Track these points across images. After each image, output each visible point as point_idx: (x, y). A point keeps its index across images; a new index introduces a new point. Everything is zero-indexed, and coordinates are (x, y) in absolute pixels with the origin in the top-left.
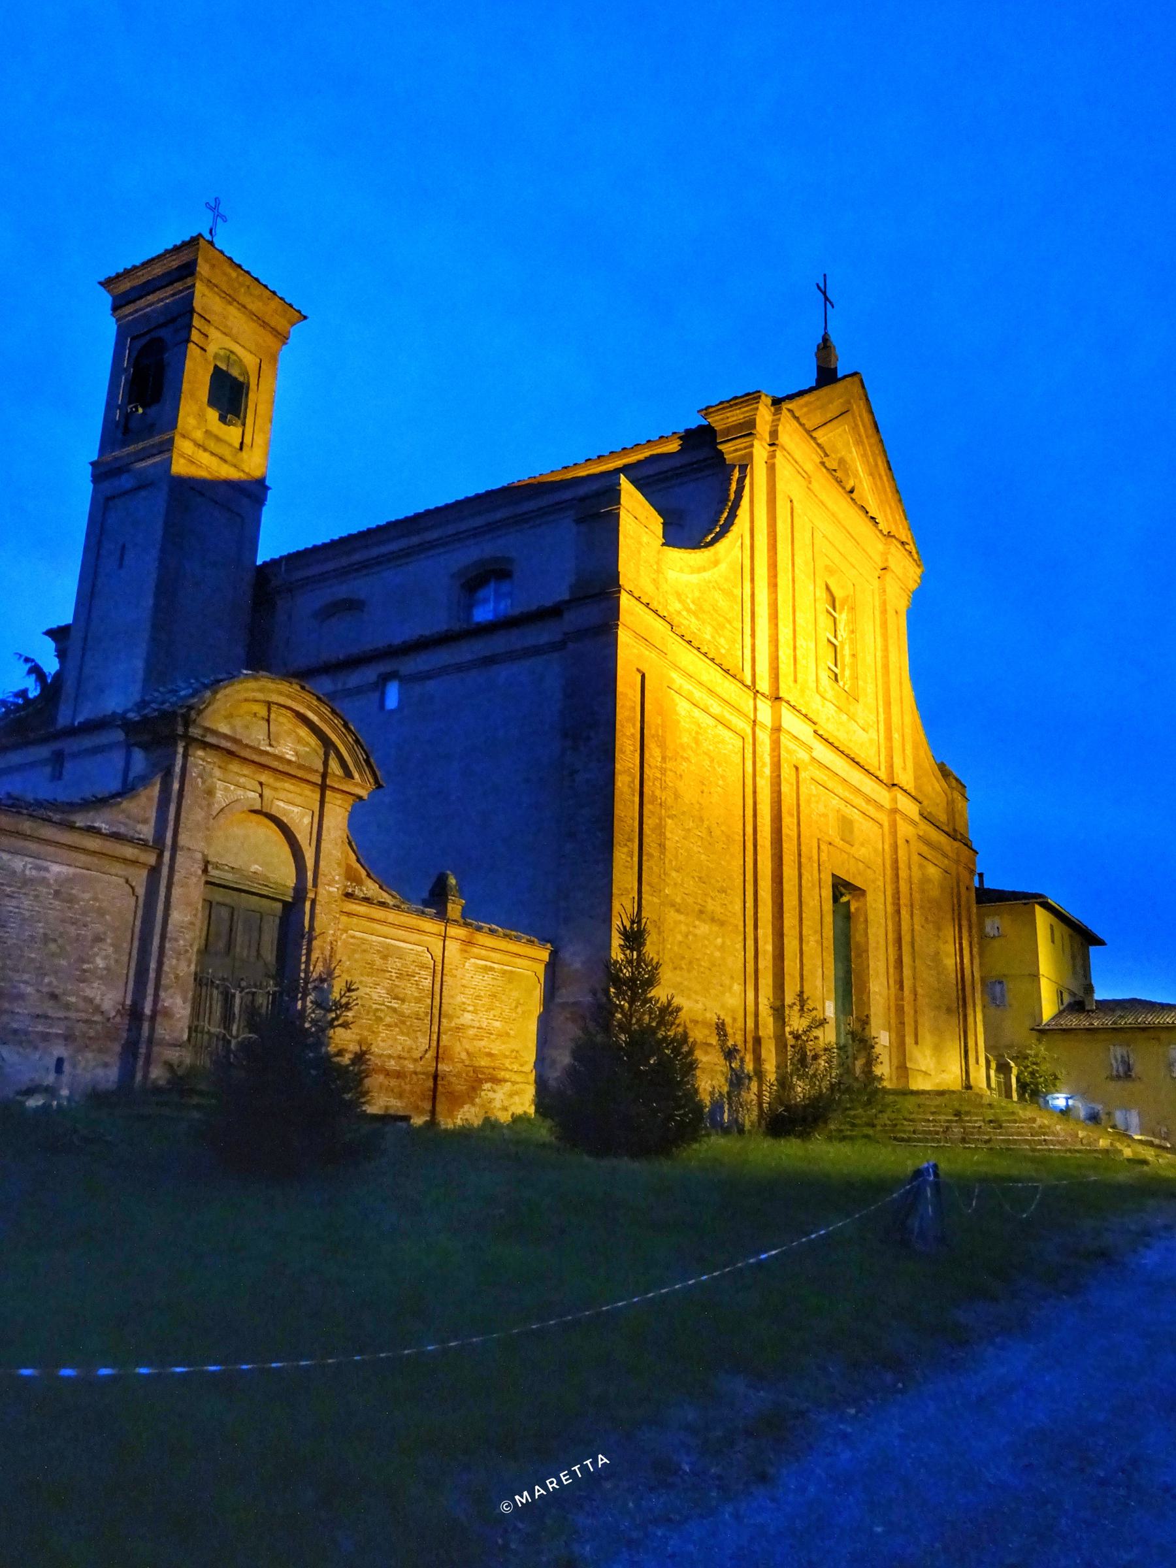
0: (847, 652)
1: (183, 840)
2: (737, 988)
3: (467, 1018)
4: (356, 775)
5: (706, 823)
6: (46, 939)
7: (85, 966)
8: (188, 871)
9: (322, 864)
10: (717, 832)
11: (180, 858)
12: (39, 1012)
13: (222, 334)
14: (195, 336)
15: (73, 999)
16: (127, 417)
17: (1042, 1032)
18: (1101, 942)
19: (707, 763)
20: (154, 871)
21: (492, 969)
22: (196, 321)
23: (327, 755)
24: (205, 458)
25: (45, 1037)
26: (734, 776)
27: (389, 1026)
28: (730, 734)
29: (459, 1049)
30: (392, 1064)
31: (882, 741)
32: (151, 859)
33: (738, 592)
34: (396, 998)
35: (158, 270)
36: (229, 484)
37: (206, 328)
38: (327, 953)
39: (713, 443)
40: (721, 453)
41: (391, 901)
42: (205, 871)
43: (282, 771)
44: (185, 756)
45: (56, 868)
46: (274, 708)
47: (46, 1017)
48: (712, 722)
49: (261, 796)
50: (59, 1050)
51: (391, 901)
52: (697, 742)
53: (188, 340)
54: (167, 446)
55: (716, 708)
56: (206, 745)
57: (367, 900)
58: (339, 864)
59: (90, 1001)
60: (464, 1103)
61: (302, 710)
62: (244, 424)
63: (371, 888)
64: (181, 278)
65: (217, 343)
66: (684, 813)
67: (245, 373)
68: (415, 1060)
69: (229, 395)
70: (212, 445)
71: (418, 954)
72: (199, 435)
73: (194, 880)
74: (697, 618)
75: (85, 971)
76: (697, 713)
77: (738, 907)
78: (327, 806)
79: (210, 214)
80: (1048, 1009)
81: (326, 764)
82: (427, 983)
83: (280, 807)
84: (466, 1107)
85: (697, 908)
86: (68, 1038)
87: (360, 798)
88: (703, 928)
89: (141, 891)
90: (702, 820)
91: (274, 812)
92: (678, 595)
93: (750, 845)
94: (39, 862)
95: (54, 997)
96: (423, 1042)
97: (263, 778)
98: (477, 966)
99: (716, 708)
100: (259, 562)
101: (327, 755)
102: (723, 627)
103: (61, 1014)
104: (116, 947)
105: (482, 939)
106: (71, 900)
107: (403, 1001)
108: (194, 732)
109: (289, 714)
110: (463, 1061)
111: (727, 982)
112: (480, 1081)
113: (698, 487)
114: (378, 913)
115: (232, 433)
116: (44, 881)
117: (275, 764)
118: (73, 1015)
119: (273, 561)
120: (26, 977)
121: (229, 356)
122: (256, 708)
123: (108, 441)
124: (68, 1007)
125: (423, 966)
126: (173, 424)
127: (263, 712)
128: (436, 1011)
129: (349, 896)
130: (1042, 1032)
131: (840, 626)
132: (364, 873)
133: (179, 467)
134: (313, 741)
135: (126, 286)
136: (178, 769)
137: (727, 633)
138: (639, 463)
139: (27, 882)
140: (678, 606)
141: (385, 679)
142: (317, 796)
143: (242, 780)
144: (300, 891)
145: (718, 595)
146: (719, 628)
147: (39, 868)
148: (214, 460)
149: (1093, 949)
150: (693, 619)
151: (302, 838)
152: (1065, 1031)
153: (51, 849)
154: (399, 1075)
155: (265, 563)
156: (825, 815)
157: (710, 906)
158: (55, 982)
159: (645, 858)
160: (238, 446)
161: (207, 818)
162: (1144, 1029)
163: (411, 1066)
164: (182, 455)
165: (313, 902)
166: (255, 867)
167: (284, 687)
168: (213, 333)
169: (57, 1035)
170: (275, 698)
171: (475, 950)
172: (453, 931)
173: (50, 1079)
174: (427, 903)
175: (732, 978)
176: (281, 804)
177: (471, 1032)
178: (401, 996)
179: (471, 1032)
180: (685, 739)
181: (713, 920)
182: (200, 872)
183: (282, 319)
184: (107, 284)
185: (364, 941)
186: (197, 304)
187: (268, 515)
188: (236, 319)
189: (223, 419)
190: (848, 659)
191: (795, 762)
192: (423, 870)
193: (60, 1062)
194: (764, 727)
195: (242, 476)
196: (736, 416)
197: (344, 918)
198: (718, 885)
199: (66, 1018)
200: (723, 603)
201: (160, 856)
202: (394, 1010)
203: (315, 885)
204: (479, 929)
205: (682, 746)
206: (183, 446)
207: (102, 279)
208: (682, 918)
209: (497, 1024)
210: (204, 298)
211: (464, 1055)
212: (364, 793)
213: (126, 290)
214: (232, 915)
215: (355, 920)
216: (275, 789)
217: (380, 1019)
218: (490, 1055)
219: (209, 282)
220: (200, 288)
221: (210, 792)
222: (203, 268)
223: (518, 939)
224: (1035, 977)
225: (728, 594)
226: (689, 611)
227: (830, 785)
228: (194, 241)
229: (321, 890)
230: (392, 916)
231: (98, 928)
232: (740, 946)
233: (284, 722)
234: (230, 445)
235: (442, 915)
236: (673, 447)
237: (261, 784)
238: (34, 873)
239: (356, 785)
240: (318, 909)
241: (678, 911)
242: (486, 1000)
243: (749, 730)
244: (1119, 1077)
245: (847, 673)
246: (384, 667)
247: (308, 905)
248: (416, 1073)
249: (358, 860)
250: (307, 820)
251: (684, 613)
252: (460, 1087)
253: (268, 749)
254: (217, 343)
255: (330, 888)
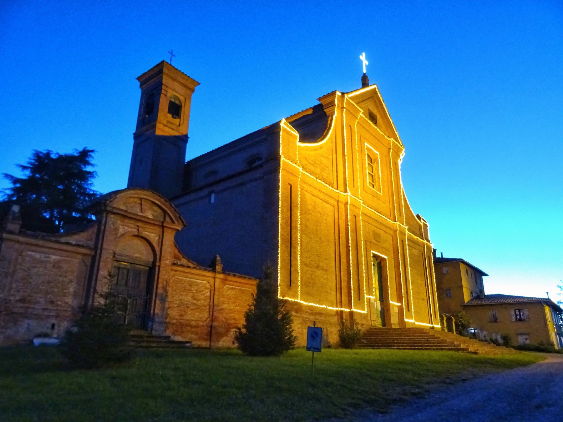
0: (377, 177)
1: (105, 246)
2: (334, 293)
3: (225, 306)
4: (176, 222)
5: (319, 236)
6: (49, 282)
7: (65, 291)
8: (106, 256)
9: (163, 253)
10: (323, 239)
11: (103, 252)
12: (46, 307)
13: (171, 90)
14: (163, 91)
15: (59, 303)
16: (144, 119)
17: (465, 306)
18: (486, 275)
19: (319, 215)
20: (94, 257)
21: (235, 289)
22: (163, 87)
23: (165, 216)
24: (167, 129)
25: (48, 317)
26: (330, 220)
27: (192, 310)
28: (329, 205)
29: (221, 317)
30: (193, 323)
31: (391, 206)
32: (93, 253)
33: (331, 157)
34: (195, 299)
35: (152, 73)
36: (175, 137)
37: (167, 89)
38: (165, 284)
39: (323, 109)
40: (325, 112)
41: (192, 266)
42: (114, 256)
43: (146, 222)
44: (106, 217)
45: (54, 257)
46: (143, 200)
47: (48, 309)
48: (321, 201)
49: (138, 230)
50: (54, 321)
51: (192, 266)
52: (314, 208)
53: (161, 93)
54: (154, 127)
55: (322, 196)
56: (114, 213)
57: (182, 266)
58: (170, 253)
59: (67, 303)
60: (224, 336)
61: (154, 200)
62: (180, 118)
63: (184, 261)
64: (159, 74)
65: (170, 93)
66: (309, 233)
67: (180, 101)
68: (203, 322)
69: (176, 110)
70: (169, 125)
71: (204, 284)
72: (165, 122)
73: (109, 260)
74: (314, 166)
75: (65, 293)
76: (314, 198)
77: (333, 264)
78: (165, 234)
79: (170, 55)
80: (467, 298)
81: (165, 219)
82: (208, 294)
83: (146, 234)
84: (224, 338)
85: (316, 265)
86: (57, 317)
87: (178, 230)
88: (319, 272)
89: (89, 264)
90: (317, 235)
91: (143, 235)
92: (306, 159)
93: (337, 243)
94: (47, 255)
95: (52, 302)
96: (206, 315)
97: (139, 224)
98: (228, 287)
99: (322, 196)
100: (186, 161)
101: (165, 216)
102: (325, 169)
103: (55, 308)
104: (78, 284)
105: (230, 278)
106: (60, 267)
107: (198, 300)
108: (108, 208)
109: (149, 202)
110: (223, 321)
111: (329, 291)
112: (230, 328)
113: (313, 124)
114: (188, 270)
115: (177, 121)
116: (50, 262)
117: (143, 219)
118: (59, 308)
119: (191, 161)
120: (40, 295)
121: (175, 97)
122: (136, 200)
123: (138, 127)
124: (57, 305)
125: (206, 288)
126: (156, 119)
127: (139, 202)
128: (211, 304)
129: (174, 264)
130: (466, 307)
131: (374, 169)
132: (181, 256)
133: (158, 132)
134: (159, 211)
135: (144, 79)
136: (103, 221)
137: (326, 171)
138: (300, 118)
139: (42, 262)
140: (306, 162)
141: (210, 193)
142: (161, 230)
143: (130, 225)
144: (154, 263)
145: (322, 158)
146: (323, 169)
147: (45, 257)
148: (170, 130)
149: (484, 277)
150: (312, 166)
151: (155, 245)
152: (475, 306)
153: (52, 251)
154: (196, 327)
155: (188, 162)
156: (369, 233)
157: (321, 264)
158: (52, 297)
159: (292, 248)
160: (178, 124)
161: (115, 239)
162: (501, 304)
163: (201, 324)
164: (159, 128)
165: (159, 266)
166: (136, 255)
167: (146, 193)
168: (169, 91)
169: (53, 316)
170: (142, 196)
171: (229, 282)
172: (218, 276)
173: (49, 331)
174: (210, 267)
175: (331, 289)
176: (147, 233)
177: (226, 311)
178: (197, 298)
179: (226, 311)
180: (310, 207)
181: (322, 269)
182: (111, 257)
183: (190, 85)
184: (138, 79)
185: (181, 280)
186: (164, 82)
187: (189, 146)
188: (177, 86)
189: (173, 117)
190: (377, 180)
191: (354, 214)
192: (199, 253)
193: (53, 326)
194: (342, 202)
195: (179, 134)
196: (329, 100)
197: (173, 272)
198: (324, 257)
199: (57, 310)
200: (325, 161)
201: (96, 251)
202: (194, 304)
203: (160, 260)
204: (229, 275)
205: (308, 209)
206: (159, 125)
207: (137, 77)
208: (309, 269)
209: (238, 308)
210: (166, 80)
211: (223, 319)
212: (180, 229)
213: (144, 80)
214: (128, 272)
215: (178, 273)
216: (143, 228)
217: (188, 307)
218: (234, 319)
219: (168, 75)
220: (164, 76)
221: (116, 229)
222: (165, 70)
223: (245, 278)
224: (461, 287)
225: (327, 158)
226: (310, 164)
227: (370, 222)
228: (162, 63)
229: (162, 262)
230: (193, 271)
231: (71, 278)
232: (334, 278)
233: (146, 205)
234: (175, 124)
235: (214, 270)
236: (310, 112)
237: (138, 226)
238: (45, 259)
239: (176, 226)
240: (161, 269)
241: (307, 266)
242: (233, 300)
243: (336, 204)
244: (492, 322)
245: (377, 184)
246: (211, 189)
247: (157, 268)
248: (203, 326)
249: (179, 252)
250: (157, 238)
251: (309, 165)
252: (222, 330)
253: (141, 214)
254: (170, 93)
255: (167, 260)
